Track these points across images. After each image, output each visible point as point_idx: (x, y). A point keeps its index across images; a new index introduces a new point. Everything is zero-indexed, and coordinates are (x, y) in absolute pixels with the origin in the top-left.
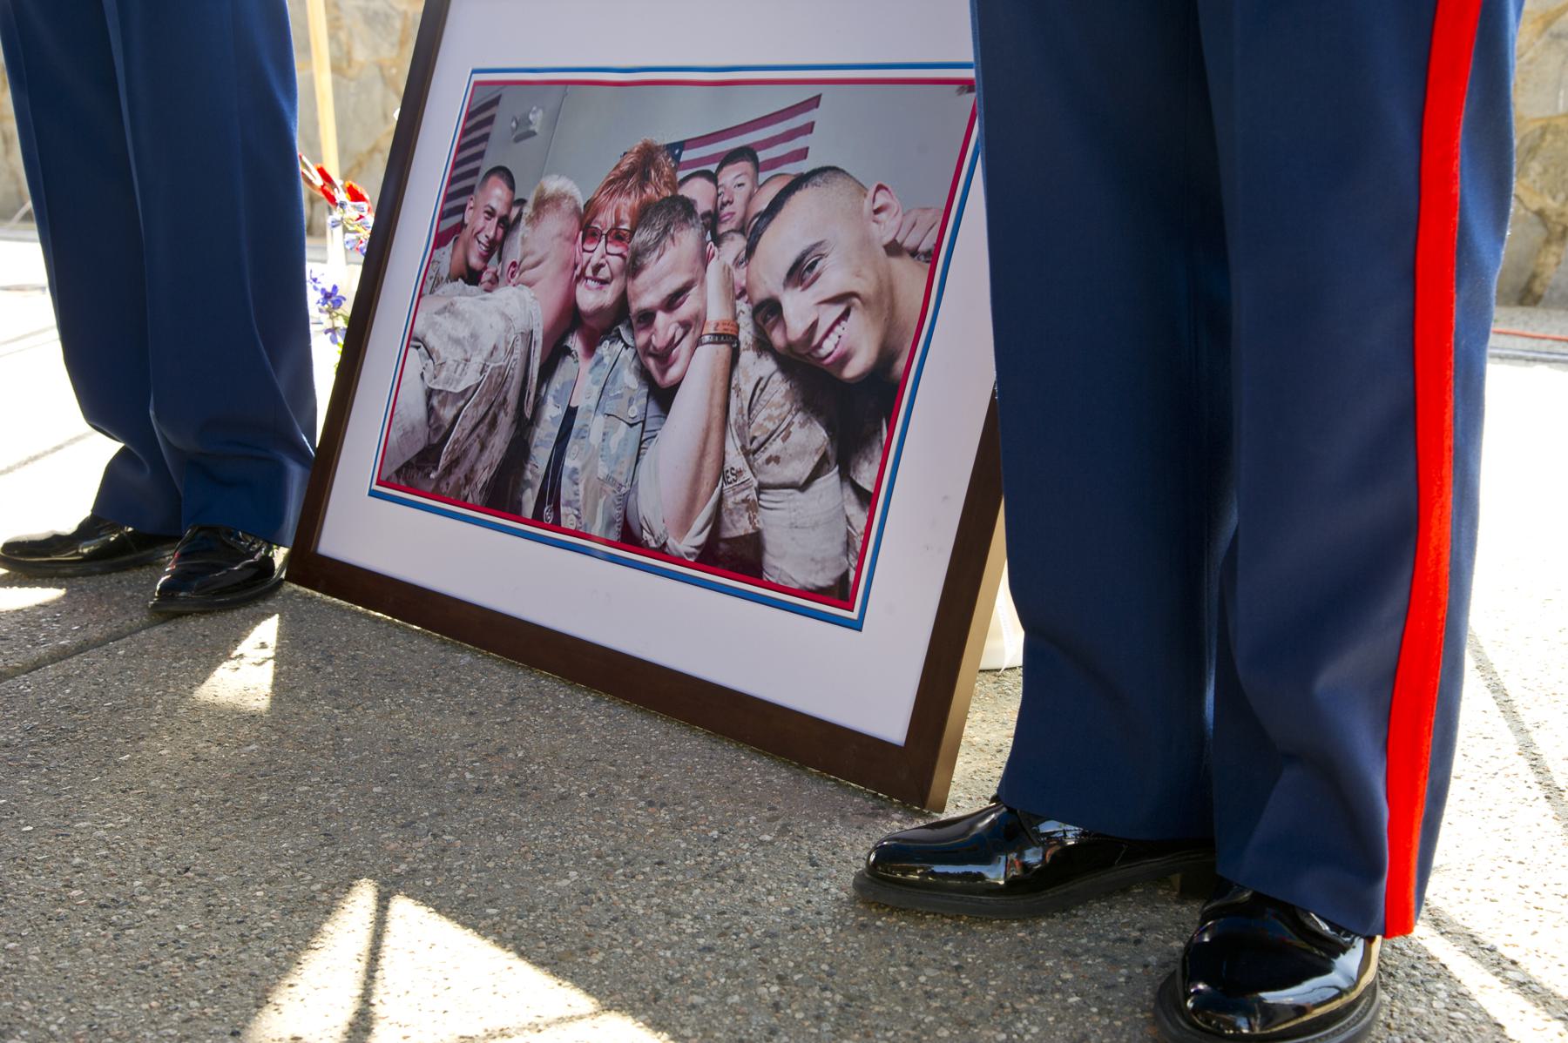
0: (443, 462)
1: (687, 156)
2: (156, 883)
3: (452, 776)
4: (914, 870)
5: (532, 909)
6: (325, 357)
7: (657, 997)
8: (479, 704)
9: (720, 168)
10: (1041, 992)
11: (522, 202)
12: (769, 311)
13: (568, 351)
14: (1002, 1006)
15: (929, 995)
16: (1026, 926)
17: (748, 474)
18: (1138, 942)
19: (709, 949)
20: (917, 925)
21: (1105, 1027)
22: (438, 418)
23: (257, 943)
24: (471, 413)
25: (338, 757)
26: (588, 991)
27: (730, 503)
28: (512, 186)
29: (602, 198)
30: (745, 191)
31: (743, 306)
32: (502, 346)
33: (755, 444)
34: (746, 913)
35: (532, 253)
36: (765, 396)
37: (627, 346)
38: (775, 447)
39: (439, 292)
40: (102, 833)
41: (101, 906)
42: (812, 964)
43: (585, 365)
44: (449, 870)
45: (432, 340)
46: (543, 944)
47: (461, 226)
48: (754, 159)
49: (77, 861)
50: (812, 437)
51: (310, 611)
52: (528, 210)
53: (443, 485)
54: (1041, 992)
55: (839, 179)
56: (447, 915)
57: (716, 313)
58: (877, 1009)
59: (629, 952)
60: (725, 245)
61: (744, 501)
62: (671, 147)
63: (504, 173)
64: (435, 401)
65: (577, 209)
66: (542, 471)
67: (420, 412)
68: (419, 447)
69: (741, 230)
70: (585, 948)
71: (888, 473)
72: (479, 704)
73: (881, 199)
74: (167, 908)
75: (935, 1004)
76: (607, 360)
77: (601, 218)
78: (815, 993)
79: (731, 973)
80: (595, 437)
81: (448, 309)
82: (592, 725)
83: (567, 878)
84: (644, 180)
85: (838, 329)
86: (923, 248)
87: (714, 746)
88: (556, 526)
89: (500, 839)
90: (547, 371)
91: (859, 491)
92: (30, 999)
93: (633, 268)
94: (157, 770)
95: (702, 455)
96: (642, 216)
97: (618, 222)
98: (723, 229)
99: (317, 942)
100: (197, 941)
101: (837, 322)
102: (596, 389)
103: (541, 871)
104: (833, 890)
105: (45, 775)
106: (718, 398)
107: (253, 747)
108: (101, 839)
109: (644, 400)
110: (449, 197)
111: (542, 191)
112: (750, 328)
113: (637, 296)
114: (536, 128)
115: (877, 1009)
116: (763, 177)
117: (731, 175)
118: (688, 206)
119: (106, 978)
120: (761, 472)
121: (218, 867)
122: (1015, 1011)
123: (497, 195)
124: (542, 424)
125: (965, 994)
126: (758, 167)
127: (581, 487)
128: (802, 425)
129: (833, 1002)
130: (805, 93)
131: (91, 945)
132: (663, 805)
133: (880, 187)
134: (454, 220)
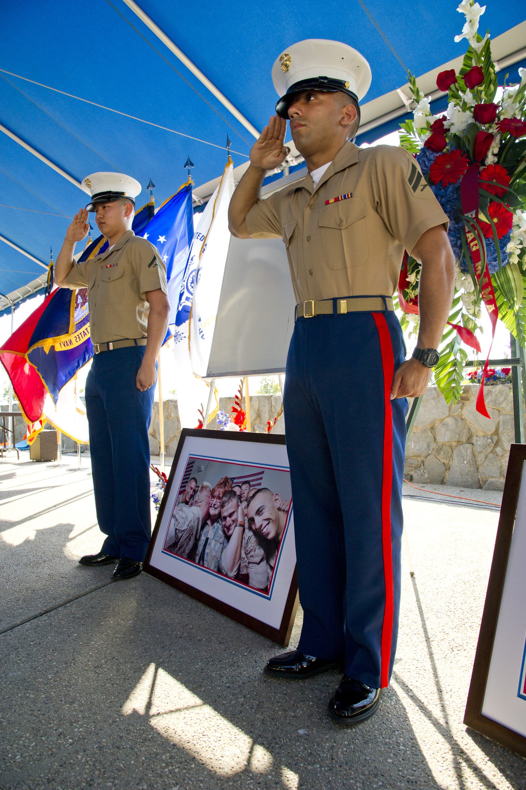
0: (178, 546)
1: (235, 481)
2: (107, 661)
3: (175, 633)
4: (278, 667)
5: (189, 674)
6: (154, 514)
7: (216, 701)
8: (183, 610)
9: (242, 485)
10: (304, 701)
11: (198, 487)
12: (252, 520)
13: (207, 524)
14: (294, 705)
15: (278, 702)
16: (303, 681)
17: (246, 559)
18: (328, 686)
19: (229, 687)
20: (278, 681)
21: (317, 711)
22: (178, 536)
23: (127, 681)
24: (185, 536)
25: (149, 626)
26: (200, 698)
27: (242, 565)
28: (196, 482)
29: (216, 488)
30: (247, 491)
31: (246, 518)
32: (192, 520)
33: (248, 552)
34: (238, 677)
35: (200, 499)
36: (250, 541)
37: (220, 524)
38: (252, 553)
39: (179, 505)
40: (96, 646)
41: (95, 667)
42: (252, 692)
43: (211, 528)
44: (172, 661)
45: (177, 517)
46: (191, 684)
47: (185, 490)
48: (249, 484)
49: (91, 653)
50: (260, 552)
51: (147, 580)
52: (200, 489)
53: (178, 552)
54: (304, 701)
55: (268, 491)
56: (170, 674)
57: (240, 519)
58: (266, 706)
59: (210, 688)
60: (243, 503)
61: (245, 565)
62: (231, 478)
63: (194, 479)
64: (177, 531)
65: (210, 490)
66: (200, 552)
67: (174, 533)
68: (173, 542)
69: (246, 500)
70: (200, 686)
71: (277, 562)
72: (183, 610)
73: (277, 497)
74: (109, 669)
75: (279, 704)
76: (216, 527)
77: (215, 493)
78: (252, 701)
79: (233, 695)
80: (212, 546)
81: (181, 510)
82: (208, 618)
83: (198, 665)
84: (225, 486)
85: (267, 527)
86: (286, 510)
87: (236, 625)
88: (203, 566)
89: (184, 652)
90: (203, 528)
91: (271, 566)
92: (79, 693)
93: (222, 506)
94: (110, 627)
95: (237, 550)
96: (225, 493)
97: (219, 495)
98: (242, 499)
99: (141, 681)
100: (115, 679)
101: (267, 525)
102: (213, 534)
103: (193, 663)
104: (259, 670)
105: (86, 628)
106: (240, 540)
107: (131, 622)
108: (96, 647)
109: (224, 538)
110: (182, 483)
111: (203, 485)
112: (247, 524)
113: (223, 513)
114: (202, 470)
115: (266, 706)
116: (251, 488)
117: (245, 487)
118: (235, 493)
119: (94, 688)
120: (249, 559)
121: (121, 657)
122: (297, 707)
123: (193, 484)
124: (201, 541)
125: (286, 702)
126: (250, 486)
127: (209, 557)
128: (258, 549)
129: (256, 704)
130: (261, 470)
131: (92, 679)
132: (223, 643)
133: (277, 494)
134: (183, 489)
